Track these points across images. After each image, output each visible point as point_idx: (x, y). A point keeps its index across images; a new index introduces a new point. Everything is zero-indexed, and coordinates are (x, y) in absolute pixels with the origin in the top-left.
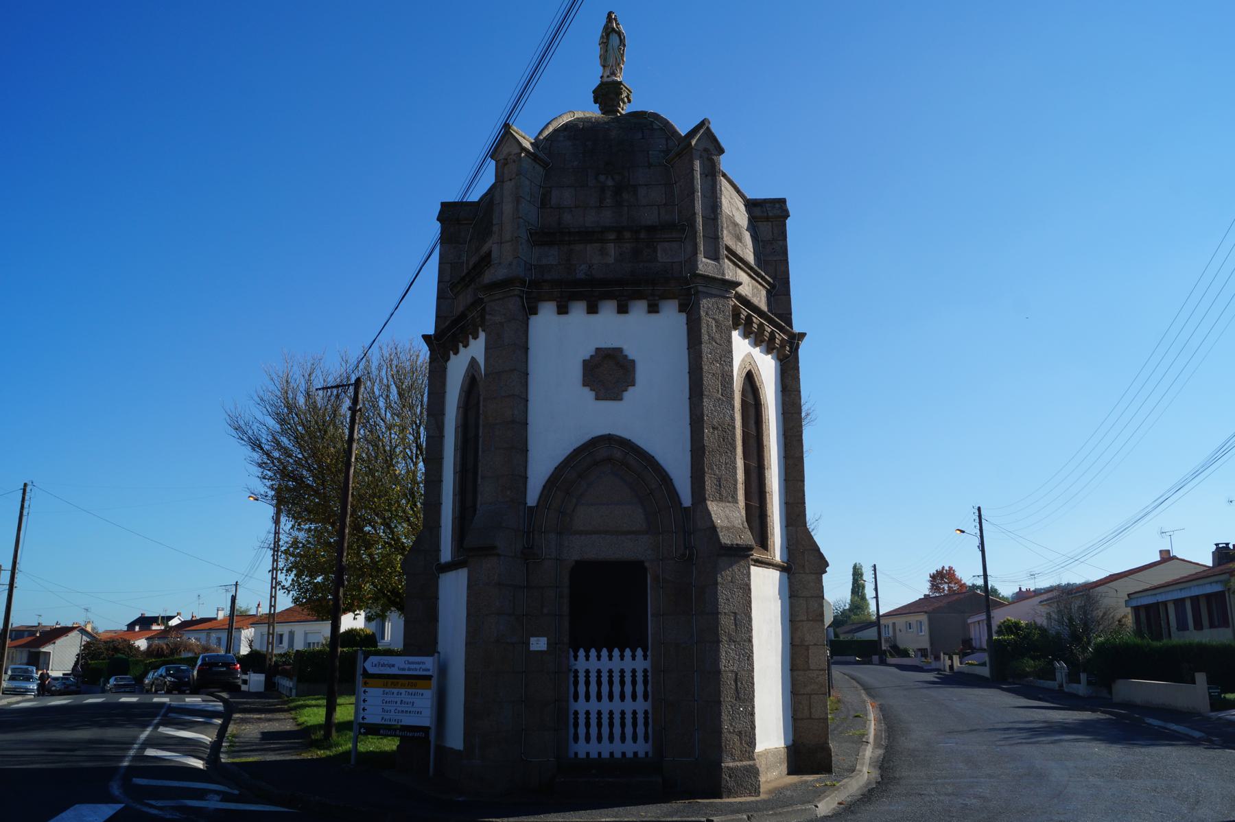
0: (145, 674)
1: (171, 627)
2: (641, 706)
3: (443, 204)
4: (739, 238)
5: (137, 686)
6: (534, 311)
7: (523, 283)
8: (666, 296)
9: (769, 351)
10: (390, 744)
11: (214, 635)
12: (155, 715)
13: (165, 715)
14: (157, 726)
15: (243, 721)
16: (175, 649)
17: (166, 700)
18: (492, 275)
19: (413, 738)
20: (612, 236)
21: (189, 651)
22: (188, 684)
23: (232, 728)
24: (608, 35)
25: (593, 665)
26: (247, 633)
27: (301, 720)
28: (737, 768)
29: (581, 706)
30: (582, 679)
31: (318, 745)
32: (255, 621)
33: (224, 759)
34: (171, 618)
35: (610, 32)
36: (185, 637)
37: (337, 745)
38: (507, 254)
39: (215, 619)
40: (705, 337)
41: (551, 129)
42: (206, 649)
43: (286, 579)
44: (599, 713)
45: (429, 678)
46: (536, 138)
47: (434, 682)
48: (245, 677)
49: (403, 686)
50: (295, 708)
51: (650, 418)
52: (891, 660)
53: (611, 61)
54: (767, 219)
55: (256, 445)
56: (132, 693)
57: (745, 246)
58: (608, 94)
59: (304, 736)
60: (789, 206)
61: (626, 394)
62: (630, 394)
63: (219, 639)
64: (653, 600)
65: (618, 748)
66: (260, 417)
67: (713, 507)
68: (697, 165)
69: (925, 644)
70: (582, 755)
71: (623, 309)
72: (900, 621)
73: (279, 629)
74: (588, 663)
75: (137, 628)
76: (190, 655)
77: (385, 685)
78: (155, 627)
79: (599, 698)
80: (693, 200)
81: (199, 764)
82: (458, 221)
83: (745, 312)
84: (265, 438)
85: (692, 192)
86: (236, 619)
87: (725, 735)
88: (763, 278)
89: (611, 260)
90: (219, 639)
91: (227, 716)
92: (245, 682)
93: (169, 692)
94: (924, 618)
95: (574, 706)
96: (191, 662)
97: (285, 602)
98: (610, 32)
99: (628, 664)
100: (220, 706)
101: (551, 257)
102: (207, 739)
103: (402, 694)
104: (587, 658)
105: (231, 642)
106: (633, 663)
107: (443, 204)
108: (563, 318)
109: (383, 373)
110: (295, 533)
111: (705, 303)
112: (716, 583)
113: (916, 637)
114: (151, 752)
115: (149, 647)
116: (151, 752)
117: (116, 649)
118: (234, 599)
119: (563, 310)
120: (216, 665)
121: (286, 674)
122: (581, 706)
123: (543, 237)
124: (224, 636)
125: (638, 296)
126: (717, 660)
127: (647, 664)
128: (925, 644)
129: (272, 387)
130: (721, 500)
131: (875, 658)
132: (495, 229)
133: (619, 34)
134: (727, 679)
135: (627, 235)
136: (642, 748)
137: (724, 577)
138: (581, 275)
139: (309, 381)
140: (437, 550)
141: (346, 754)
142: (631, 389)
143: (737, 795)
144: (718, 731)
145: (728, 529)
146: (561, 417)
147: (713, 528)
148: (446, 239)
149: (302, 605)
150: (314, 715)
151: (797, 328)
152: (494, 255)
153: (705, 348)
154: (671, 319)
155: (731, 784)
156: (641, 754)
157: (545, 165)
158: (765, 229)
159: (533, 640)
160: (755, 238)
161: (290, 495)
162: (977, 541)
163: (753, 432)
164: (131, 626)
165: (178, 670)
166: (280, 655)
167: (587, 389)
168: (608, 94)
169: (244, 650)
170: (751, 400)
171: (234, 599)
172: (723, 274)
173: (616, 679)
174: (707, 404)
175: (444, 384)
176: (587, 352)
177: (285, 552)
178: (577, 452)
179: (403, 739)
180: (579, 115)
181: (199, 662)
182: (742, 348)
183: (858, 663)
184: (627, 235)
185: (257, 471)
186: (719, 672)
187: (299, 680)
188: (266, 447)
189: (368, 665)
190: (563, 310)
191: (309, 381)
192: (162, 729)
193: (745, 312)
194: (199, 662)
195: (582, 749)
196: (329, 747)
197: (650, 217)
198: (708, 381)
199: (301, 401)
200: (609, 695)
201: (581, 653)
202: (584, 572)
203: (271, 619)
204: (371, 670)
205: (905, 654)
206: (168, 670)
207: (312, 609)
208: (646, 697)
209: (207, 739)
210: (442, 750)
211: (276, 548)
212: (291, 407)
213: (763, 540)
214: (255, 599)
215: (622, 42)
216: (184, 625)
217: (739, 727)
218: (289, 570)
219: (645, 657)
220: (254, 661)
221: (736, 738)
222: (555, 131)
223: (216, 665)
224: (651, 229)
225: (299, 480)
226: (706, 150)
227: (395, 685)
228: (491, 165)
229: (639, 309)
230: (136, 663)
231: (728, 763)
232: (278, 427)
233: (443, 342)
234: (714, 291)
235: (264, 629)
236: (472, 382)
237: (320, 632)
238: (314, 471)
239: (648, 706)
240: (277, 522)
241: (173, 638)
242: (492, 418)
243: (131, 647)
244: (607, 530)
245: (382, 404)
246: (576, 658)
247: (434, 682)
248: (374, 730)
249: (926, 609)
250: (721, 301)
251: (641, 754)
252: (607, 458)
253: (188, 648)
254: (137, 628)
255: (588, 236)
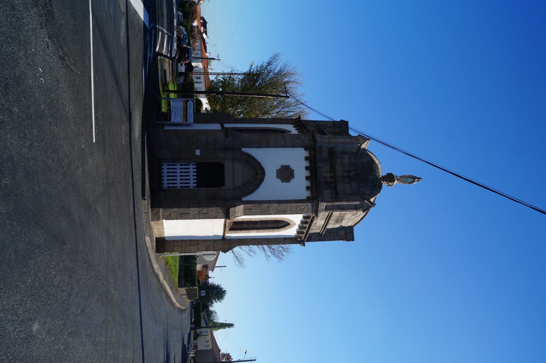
0: (184, 26)
1: (202, 35)
2: (179, 185)
3: (347, 122)
4: (337, 221)
5: (180, 23)
6: (306, 149)
7: (315, 145)
8: (312, 192)
9: (298, 232)
10: (164, 110)
11: (199, 52)
12: (170, 33)
13: (171, 36)
14: (167, 34)
15: (169, 64)
16: (193, 37)
17: (175, 36)
18: (318, 137)
19: (167, 116)
20: (332, 175)
21: (193, 43)
22: (180, 43)
23: (167, 60)
24: (412, 178)
25: (191, 170)
26: (200, 65)
27: (170, 83)
28: (159, 213)
29: (178, 167)
30: (187, 167)
31: (163, 88)
32: (206, 68)
33: (159, 57)
34: (206, 34)
35: (414, 178)
36: (198, 41)
37: (163, 94)
38: (323, 141)
39: (206, 52)
40: (298, 205)
41: (372, 155)
42: (194, 49)
43: (220, 78)
44: (176, 172)
45: (186, 121)
46: (367, 150)
47: (185, 122)
48: (183, 65)
49: (184, 113)
50: (173, 82)
51: (271, 187)
52: (192, 332)
53: (403, 179)
54: (346, 234)
55: (269, 64)
56: (177, 22)
57: (334, 224)
58: (390, 178)
59: (165, 84)
60: (351, 242)
61: (279, 179)
62: (279, 181)
63: (198, 54)
64: (212, 190)
65: (165, 178)
66: (280, 65)
67: (242, 207)
68: (358, 203)
69: (199, 348)
70: (163, 167)
71: (307, 178)
72: (209, 338)
73: (202, 77)
74: (192, 168)
75: (202, 21)
76: (191, 43)
77: (184, 107)
78: (202, 28)
79: (181, 172)
80: (345, 201)
81: (157, 50)
82: (342, 127)
83: (309, 221)
84: (273, 66)
85: (348, 201)
86: (207, 61)
87: (170, 210)
88: (323, 231)
89: (324, 174)
90: (198, 54)
91: (170, 58)
92: (182, 65)
93: (177, 36)
94: (210, 348)
95: (178, 164)
96: (189, 44)
97: (212, 78)
98: (414, 178)
99: (192, 181)
100: (173, 55)
101: (325, 155)
102: (164, 51)
103: (181, 112)
104: (194, 168)
105: (197, 59)
106: (192, 184)
107: (347, 122)
108: (304, 159)
109: (298, 110)
110: (237, 79)
111: (310, 205)
112: (217, 207)
113: (202, 344)
114: (160, 33)
115: (194, 27)
116: (160, 33)
117: (193, 14)
118: (214, 59)
119: (306, 159)
120: (188, 53)
121: (185, 80)
122: (178, 167)
123: (332, 152)
124: (199, 56)
125: (312, 183)
126: (193, 207)
127: (191, 187)
128: (199, 348)
129: (291, 68)
130: (244, 210)
131: (193, 326)
132: (334, 136)
133: (413, 182)
134: (186, 210)
135: (333, 180)
136: (165, 186)
137: (219, 210)
138: (319, 165)
139: (293, 82)
140: (228, 123)
141: (161, 96)
142: (280, 181)
143: (152, 213)
144: (171, 207)
145: (235, 211)
146: (271, 158)
147: (235, 206)
148: (334, 123)
149: (211, 83)
150: (171, 87)
151: (306, 243)
152: (325, 136)
153: (294, 205)
154: (304, 194)
155: (155, 211)
156: (163, 186)
157: (357, 153)
158: (342, 233)
159: (199, 151)
160: (338, 229)
161: (251, 77)
162: (242, 359)
163: (269, 226)
164: (203, 18)
165: (186, 39)
166: (192, 78)
167: (280, 167)
168: (390, 178)
169: (194, 64)
170: (280, 225)
171: (214, 59)
172: (320, 212)
173: (187, 178)
174: (276, 205)
175: (284, 123)
176: (292, 167)
177: (230, 77)
178: (259, 164)
179: (166, 114)
180: (379, 166)
181: (189, 47)
182: (296, 219)
183: (191, 320)
184: (333, 180)
185: (259, 65)
186: (189, 207)
187: (183, 84)
188: (269, 67)
189: (190, 102)
190: (306, 159)
191: (293, 82)
192: (166, 36)
193: (309, 221)
194: (189, 47)
195: (165, 167)
196: (162, 91)
197: (340, 188)
198: (284, 206)
199: (286, 80)
200: (181, 175)
201: (195, 167)
202: (220, 167)
203: (206, 73)
204: (188, 103)
205: (195, 339)
206: (186, 35)
207: (209, 87)
208: (181, 187)
209: (164, 51)
210: (164, 125)
211: (232, 74)
212: (285, 75)
213: (232, 229)
214: (215, 67)
215: (410, 183)
216: (203, 40)
217: (172, 214)
218: (223, 78)
219: (194, 187)
220: (190, 68)
221: (169, 213)
222: (371, 157)
223: (188, 53)
224: (335, 188)
225: (257, 81)
226: (364, 206)
227: (184, 110)
228: (357, 135)
229: (307, 183)
230: (188, 22)
231: (161, 210)
232: (276, 71)
233: (298, 123)
234: (314, 208)
235: (202, 71)
236: (282, 131)
237: (200, 86)
238: (261, 85)
239: (179, 187)
240: (243, 74)
241: (198, 36)
242: (273, 138)
243: (194, 20)
244: (234, 174)
245: (287, 109)
246: (194, 165)
247: (185, 122)
248: (169, 104)
249: (214, 349)
250: (311, 210)
251: (163, 186)
252: (257, 174)
253: (194, 42)
254: (202, 21)
255: (332, 167)
